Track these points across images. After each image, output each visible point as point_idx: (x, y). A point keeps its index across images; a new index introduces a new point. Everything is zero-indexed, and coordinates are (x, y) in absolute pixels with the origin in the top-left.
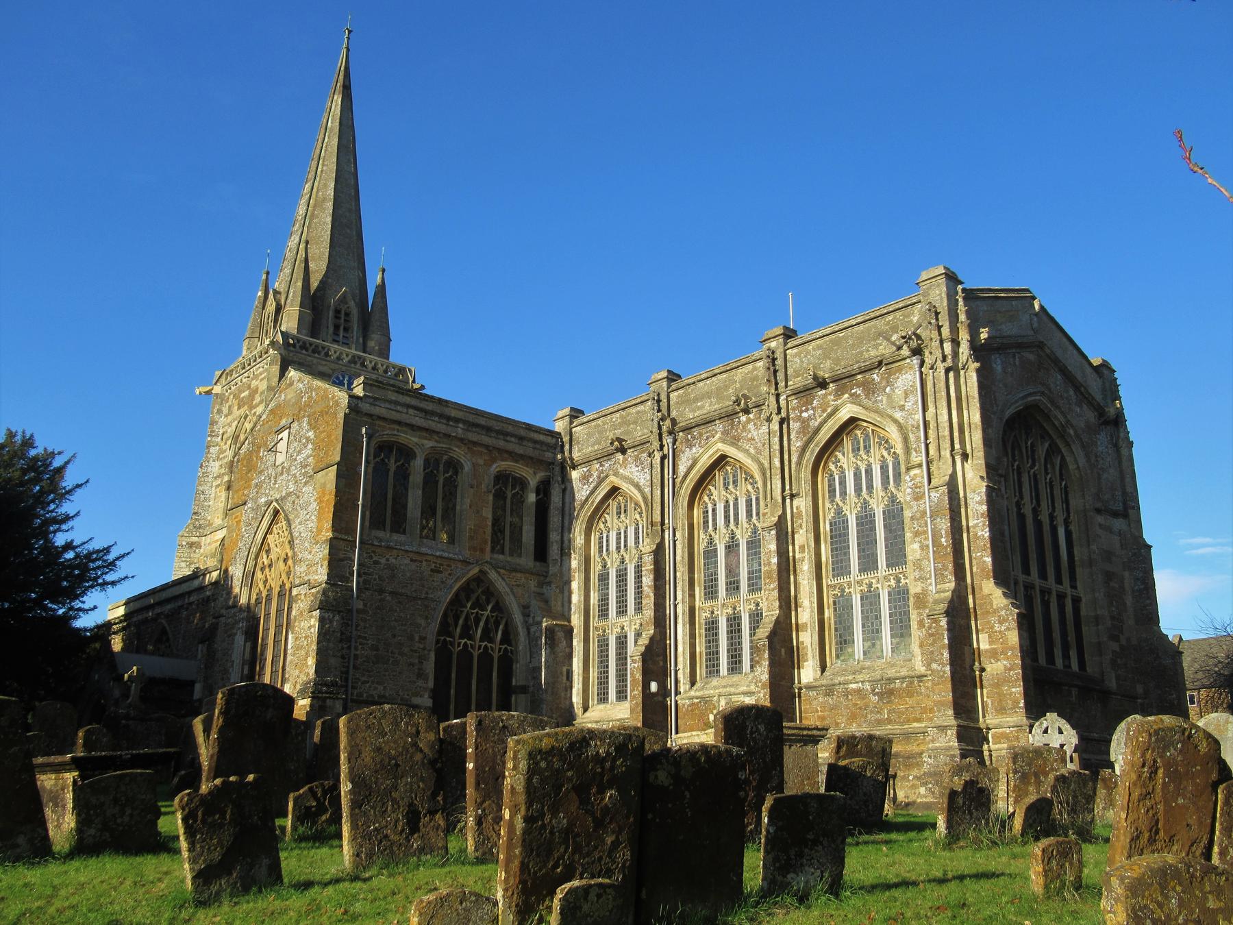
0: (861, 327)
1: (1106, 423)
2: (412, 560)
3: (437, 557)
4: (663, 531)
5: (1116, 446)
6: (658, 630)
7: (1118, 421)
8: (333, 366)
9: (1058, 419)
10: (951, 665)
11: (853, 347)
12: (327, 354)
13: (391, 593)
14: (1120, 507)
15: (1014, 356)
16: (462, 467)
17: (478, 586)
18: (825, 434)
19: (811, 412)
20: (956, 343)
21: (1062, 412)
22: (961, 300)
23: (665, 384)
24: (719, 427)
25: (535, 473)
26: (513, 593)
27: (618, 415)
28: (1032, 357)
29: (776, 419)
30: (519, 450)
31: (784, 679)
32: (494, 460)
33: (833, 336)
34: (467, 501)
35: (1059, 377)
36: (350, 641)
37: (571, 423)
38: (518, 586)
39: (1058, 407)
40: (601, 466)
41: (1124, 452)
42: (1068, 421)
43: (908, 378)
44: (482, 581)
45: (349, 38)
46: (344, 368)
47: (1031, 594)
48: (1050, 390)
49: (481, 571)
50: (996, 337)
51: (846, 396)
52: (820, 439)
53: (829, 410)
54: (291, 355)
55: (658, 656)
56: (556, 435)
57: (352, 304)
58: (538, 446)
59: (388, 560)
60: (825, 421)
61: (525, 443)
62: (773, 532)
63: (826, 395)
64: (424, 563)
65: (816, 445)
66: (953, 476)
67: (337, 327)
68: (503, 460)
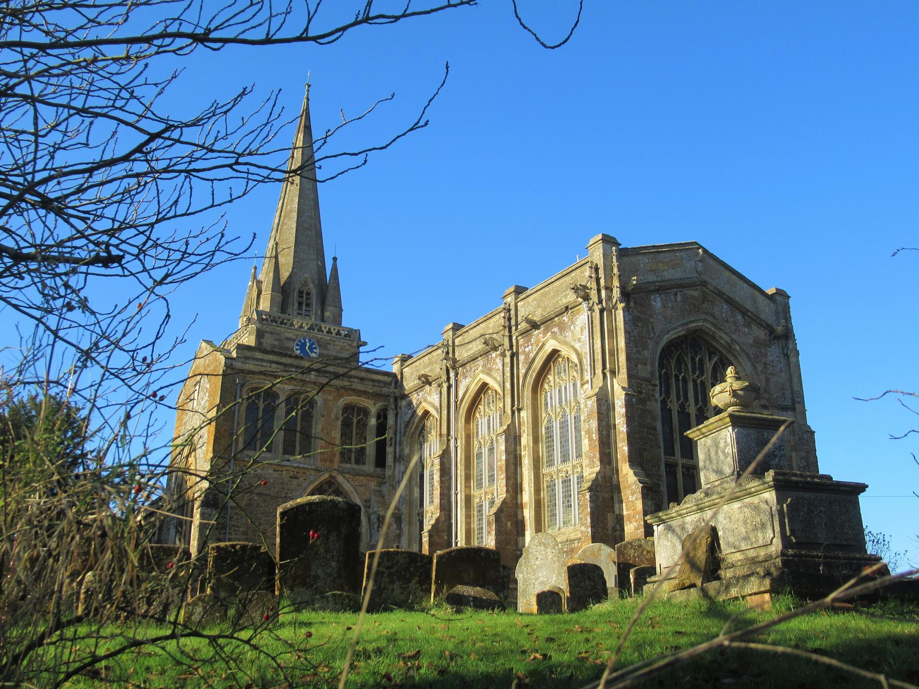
0: (558, 283)
1: (777, 338)
2: (275, 470)
3: (295, 467)
4: (448, 440)
5: (787, 356)
6: (443, 513)
7: (786, 337)
8: (296, 333)
9: (723, 339)
10: (592, 527)
11: (553, 297)
12: (292, 325)
13: (258, 494)
14: (788, 402)
15: (676, 294)
16: (316, 403)
17: (330, 487)
18: (538, 362)
19: (530, 347)
20: (609, 289)
21: (726, 333)
22: (614, 258)
23: (451, 333)
24: (481, 362)
25: (375, 404)
26: (356, 491)
27: (427, 358)
28: (695, 294)
29: (508, 354)
30: (360, 387)
31: (510, 544)
32: (341, 396)
33: (542, 291)
34: (320, 426)
35: (725, 306)
36: (225, 529)
37: (402, 365)
38: (361, 486)
39: (721, 329)
40: (418, 395)
41: (792, 359)
42: (733, 340)
43: (582, 318)
44: (333, 484)
45: (308, 91)
46: (305, 334)
47: (693, 473)
48: (714, 317)
49: (330, 476)
50: (656, 282)
51: (549, 334)
52: (536, 366)
53: (540, 345)
54: (264, 326)
55: (443, 532)
56: (394, 375)
57: (311, 286)
58: (377, 384)
59: (256, 471)
60: (537, 353)
61: (366, 382)
62: (503, 437)
63: (538, 334)
64: (284, 472)
65: (533, 371)
66: (603, 389)
67: (300, 304)
68: (349, 396)
